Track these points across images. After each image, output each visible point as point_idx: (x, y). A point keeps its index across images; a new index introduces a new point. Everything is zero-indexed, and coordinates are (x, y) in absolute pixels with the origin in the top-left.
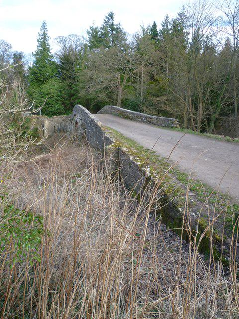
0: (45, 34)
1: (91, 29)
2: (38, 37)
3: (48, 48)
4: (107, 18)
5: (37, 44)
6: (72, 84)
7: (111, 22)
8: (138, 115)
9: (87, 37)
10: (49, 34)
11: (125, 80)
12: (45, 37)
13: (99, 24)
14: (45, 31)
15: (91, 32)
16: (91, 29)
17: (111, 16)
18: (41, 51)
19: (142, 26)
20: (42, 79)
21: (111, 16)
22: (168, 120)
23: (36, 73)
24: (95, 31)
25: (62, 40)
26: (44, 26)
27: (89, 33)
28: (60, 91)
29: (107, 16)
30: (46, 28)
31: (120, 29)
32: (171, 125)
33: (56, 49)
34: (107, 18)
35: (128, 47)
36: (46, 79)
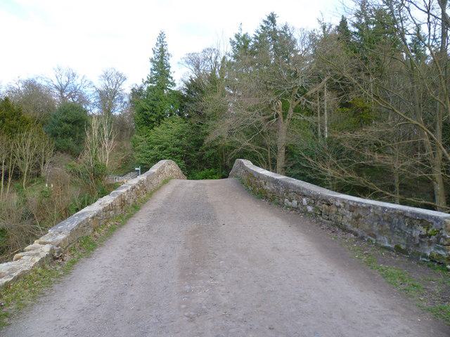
0: (162, 50)
1: (237, 37)
2: (153, 56)
3: (168, 71)
4: (265, 22)
5: (151, 66)
6: (200, 124)
7: (272, 27)
8: (287, 186)
9: (229, 49)
10: (169, 49)
11: (291, 111)
12: (163, 54)
13: (252, 29)
14: (162, 46)
15: (236, 41)
16: (237, 37)
17: (272, 19)
18: (157, 77)
19: (321, 19)
20: (153, 119)
21: (272, 19)
22: (413, 220)
23: (144, 110)
24: (245, 39)
25: (195, 62)
26: (161, 38)
27: (233, 43)
28: (180, 138)
29: (266, 19)
30: (164, 40)
31: (286, 35)
32: (429, 251)
33: (180, 76)
34: (265, 22)
35: (299, 60)
36: (160, 119)
